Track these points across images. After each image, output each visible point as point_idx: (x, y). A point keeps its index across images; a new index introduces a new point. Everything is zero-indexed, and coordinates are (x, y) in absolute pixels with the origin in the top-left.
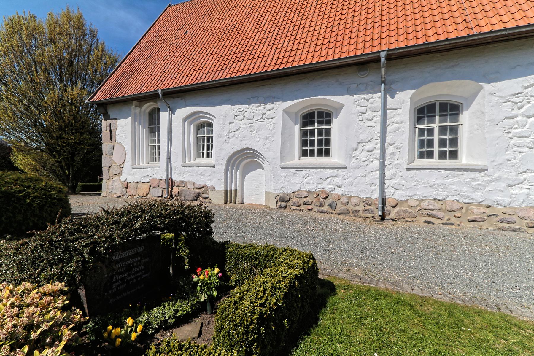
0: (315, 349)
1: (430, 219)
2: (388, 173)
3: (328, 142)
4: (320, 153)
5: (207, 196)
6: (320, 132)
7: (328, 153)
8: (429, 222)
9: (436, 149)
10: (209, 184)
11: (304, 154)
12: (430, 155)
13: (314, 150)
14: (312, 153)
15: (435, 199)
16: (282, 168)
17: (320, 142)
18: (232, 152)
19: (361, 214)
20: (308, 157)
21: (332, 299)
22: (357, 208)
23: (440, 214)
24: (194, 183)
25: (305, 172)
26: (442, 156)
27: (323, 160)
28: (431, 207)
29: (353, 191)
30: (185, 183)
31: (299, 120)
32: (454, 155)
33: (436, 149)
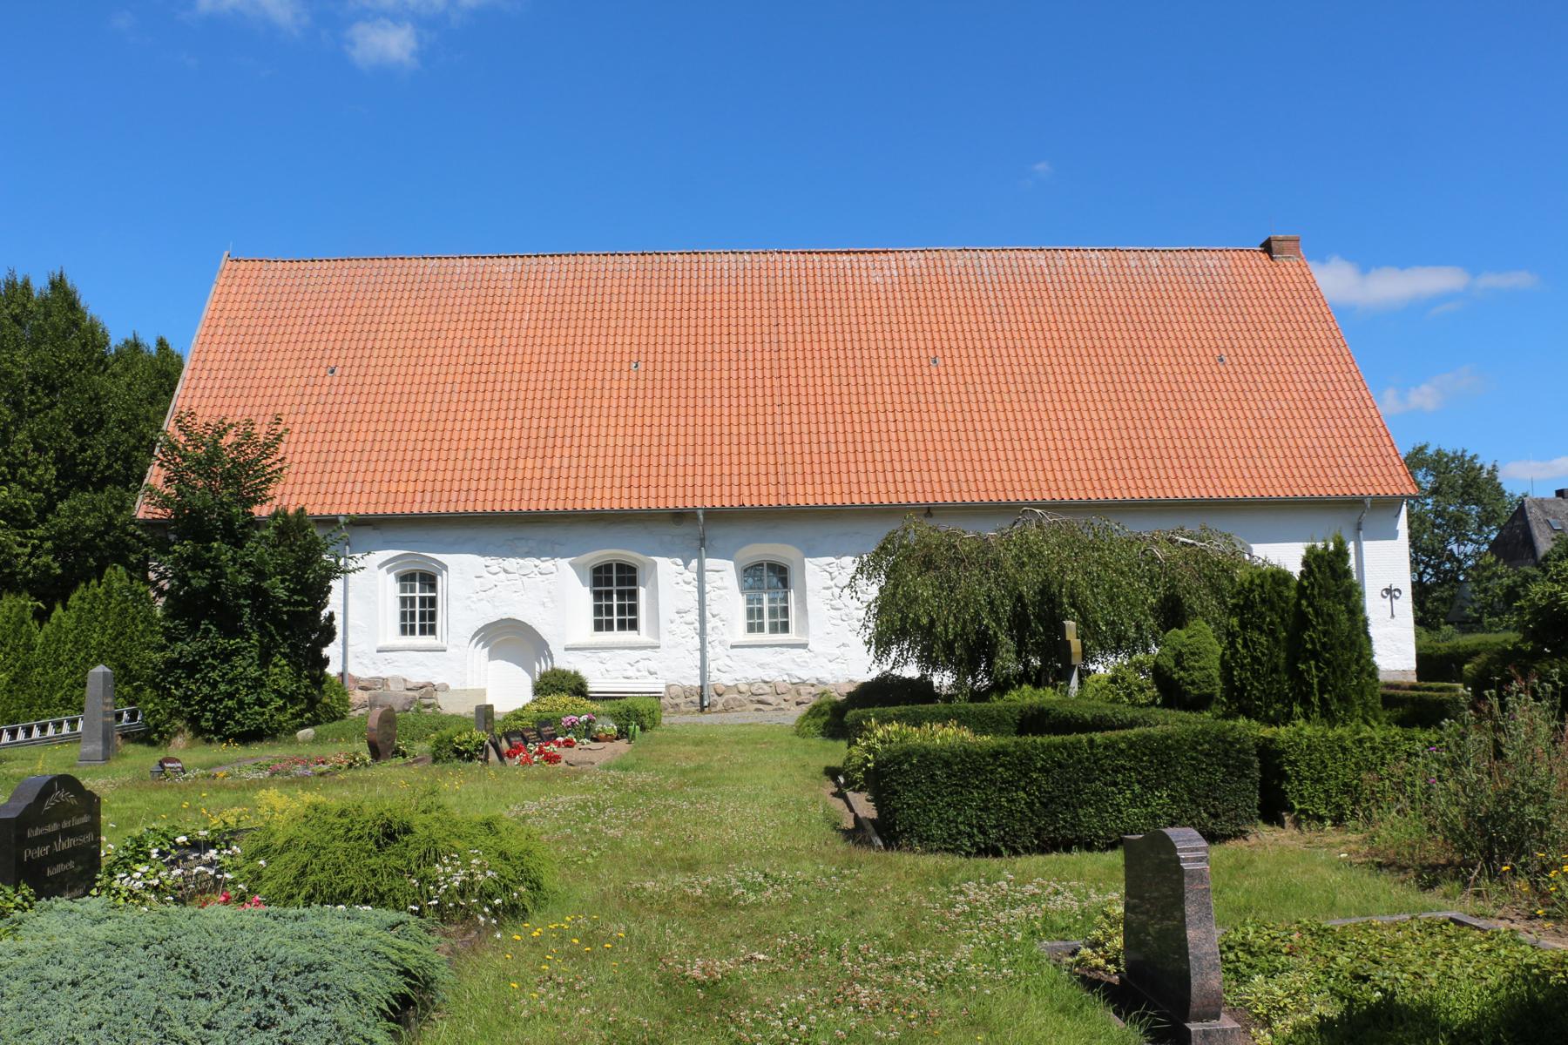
0: (344, 864)
1: (761, 706)
2: (710, 653)
3: (433, 616)
4: (622, 625)
5: (432, 701)
6: (423, 600)
7: (633, 625)
8: (757, 710)
9: (766, 621)
10: (437, 681)
11: (598, 626)
12: (761, 628)
13: (619, 614)
14: (609, 626)
15: (766, 682)
16: (566, 649)
17: (621, 610)
18: (512, 616)
19: (682, 707)
20: (604, 632)
21: (1277, 828)
22: (677, 701)
23: (770, 699)
24: (405, 680)
25: (603, 654)
26: (774, 629)
27: (628, 636)
28: (761, 691)
29: (672, 678)
30: (385, 681)
31: (589, 577)
32: (785, 627)
33: (766, 621)
